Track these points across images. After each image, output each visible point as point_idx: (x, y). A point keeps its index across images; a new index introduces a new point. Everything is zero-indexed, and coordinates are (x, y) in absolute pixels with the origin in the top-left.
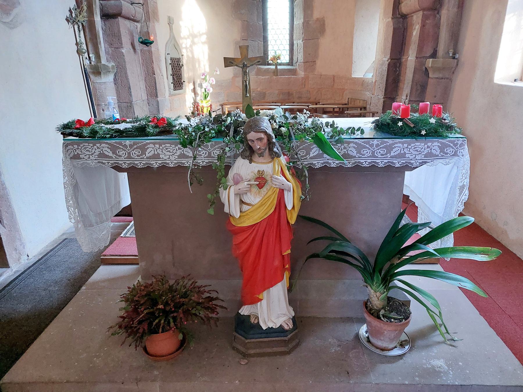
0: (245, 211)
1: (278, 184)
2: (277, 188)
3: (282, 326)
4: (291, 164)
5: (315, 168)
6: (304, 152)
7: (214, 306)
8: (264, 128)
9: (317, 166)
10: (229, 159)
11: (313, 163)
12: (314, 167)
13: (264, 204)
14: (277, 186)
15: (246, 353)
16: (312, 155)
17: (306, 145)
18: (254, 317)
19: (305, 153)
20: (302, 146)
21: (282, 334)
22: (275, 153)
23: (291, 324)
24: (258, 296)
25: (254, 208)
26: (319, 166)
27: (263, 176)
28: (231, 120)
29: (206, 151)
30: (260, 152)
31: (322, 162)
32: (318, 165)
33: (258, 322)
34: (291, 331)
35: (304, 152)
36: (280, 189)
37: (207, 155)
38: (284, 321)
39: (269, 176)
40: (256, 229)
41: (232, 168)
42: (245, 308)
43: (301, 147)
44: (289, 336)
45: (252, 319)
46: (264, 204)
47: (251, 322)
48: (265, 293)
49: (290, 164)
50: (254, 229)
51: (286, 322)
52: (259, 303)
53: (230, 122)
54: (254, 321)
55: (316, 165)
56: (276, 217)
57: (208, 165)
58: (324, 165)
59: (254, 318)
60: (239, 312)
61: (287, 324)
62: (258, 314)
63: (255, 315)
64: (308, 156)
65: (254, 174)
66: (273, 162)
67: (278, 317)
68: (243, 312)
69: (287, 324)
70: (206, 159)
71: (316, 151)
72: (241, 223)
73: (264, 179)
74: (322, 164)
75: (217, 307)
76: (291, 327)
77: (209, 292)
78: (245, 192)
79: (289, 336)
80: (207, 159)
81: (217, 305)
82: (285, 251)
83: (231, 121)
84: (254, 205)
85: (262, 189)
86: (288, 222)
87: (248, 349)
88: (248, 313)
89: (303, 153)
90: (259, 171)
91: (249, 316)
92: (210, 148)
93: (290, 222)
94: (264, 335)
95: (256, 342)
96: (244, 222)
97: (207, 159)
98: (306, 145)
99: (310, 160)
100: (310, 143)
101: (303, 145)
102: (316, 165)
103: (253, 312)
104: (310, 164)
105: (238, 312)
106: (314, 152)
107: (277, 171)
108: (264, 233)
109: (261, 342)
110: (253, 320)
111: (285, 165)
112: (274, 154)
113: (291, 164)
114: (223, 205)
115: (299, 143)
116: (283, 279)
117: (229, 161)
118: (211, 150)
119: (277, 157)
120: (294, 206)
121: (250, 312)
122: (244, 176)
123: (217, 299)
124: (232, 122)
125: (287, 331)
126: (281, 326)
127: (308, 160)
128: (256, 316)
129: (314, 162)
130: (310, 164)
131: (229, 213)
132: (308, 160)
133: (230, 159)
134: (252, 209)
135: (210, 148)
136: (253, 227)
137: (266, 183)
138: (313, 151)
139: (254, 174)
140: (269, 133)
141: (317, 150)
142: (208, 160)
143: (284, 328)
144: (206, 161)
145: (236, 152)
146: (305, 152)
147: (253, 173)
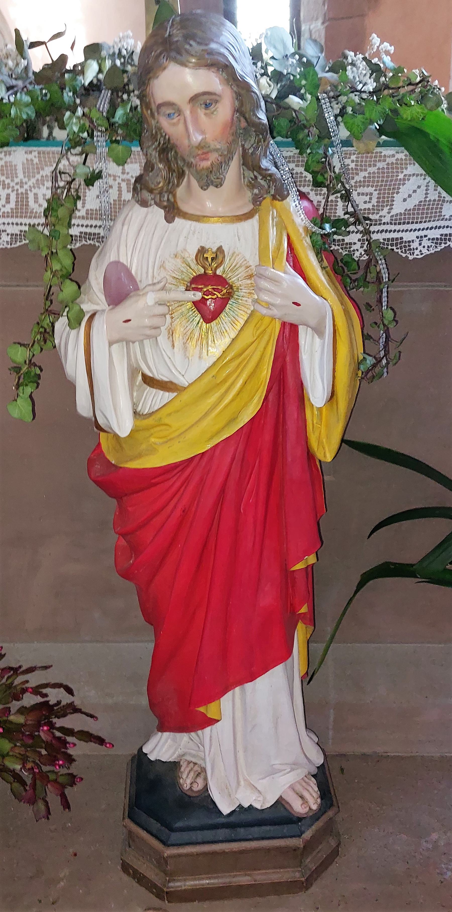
0: (151, 411)
1: (278, 301)
2: (273, 318)
3: (283, 803)
4: (327, 226)
5: (411, 257)
6: (371, 194)
7: (58, 734)
8: (223, 51)
9: (417, 252)
10: (94, 223)
11: (401, 238)
12: (404, 255)
13: (225, 380)
14: (275, 312)
15: (165, 890)
16: (399, 208)
17: (380, 165)
18: (192, 769)
19: (374, 201)
20: (366, 170)
21: (286, 829)
22: (264, 177)
23: (315, 795)
24: (202, 709)
25: (185, 397)
26: (425, 251)
27: (219, 272)
28: (100, 71)
29: (7, 191)
30: (206, 164)
31: (436, 234)
32: (420, 248)
33: (206, 788)
34: (316, 816)
35: (371, 194)
36: (284, 324)
37: (12, 205)
38: (292, 788)
39: (242, 272)
40: (196, 478)
41: (102, 249)
42: (163, 740)
43: (362, 174)
44: (308, 835)
45: (184, 776)
46: (225, 380)
47: (180, 786)
48: (226, 700)
49: (323, 229)
50: (187, 480)
51: (299, 788)
52: (208, 730)
53: (96, 77)
54: (191, 784)
55: (414, 245)
56: (267, 436)
57: (18, 244)
58: (443, 246)
59: (192, 774)
60: (145, 750)
61: (302, 797)
62: (204, 760)
63: (195, 764)
64: (386, 210)
65: (184, 261)
66: (257, 217)
67: (273, 772)
68: (155, 753)
69: (302, 797)
70: (10, 220)
71: (415, 191)
72: (139, 456)
73: (221, 281)
74: (436, 241)
75: (69, 739)
76: (314, 807)
77: (37, 691)
78: (148, 332)
79: (308, 835)
80: (15, 220)
81: (69, 732)
82: (300, 559)
83: (98, 73)
84: (185, 388)
85: (214, 323)
86: (310, 456)
87: (171, 875)
88: (172, 755)
89: (367, 198)
90: (202, 251)
91: (175, 766)
92: (21, 175)
93: (319, 455)
94: (222, 833)
95: (198, 854)
96: (152, 450)
97: (15, 220)
98: (380, 165)
99: (393, 227)
100: (393, 160)
101: (370, 166)
102: (414, 245)
103: (190, 754)
104: (392, 245)
105: (141, 749)
106: (410, 196)
107: (274, 252)
108: (230, 470)
109: (214, 853)
110: (189, 781)
111: (306, 229)
112: (263, 182)
113: (327, 226)
114: (72, 387)
115: (353, 157)
116: (289, 653)
117: (97, 231)
118: (26, 187)
119: (274, 198)
120: (333, 395)
121: (179, 752)
122: (147, 272)
123: (72, 708)
124: (101, 76)
125: (300, 819)
126: (280, 803)
127: (384, 227)
128: (200, 766)
129: (407, 237)
130: (392, 245)
131: (94, 419)
132: (384, 227)
133: (99, 223)
134: (177, 404)
135: (21, 175)
136: (183, 470)
137: (229, 299)
138: (405, 190)
139: (184, 261)
140: (241, 76)
141: (419, 187)
142: (17, 224)
143: (292, 808)
144: (11, 230)
145: (120, 195)
146: (375, 194)
147: (179, 261)
